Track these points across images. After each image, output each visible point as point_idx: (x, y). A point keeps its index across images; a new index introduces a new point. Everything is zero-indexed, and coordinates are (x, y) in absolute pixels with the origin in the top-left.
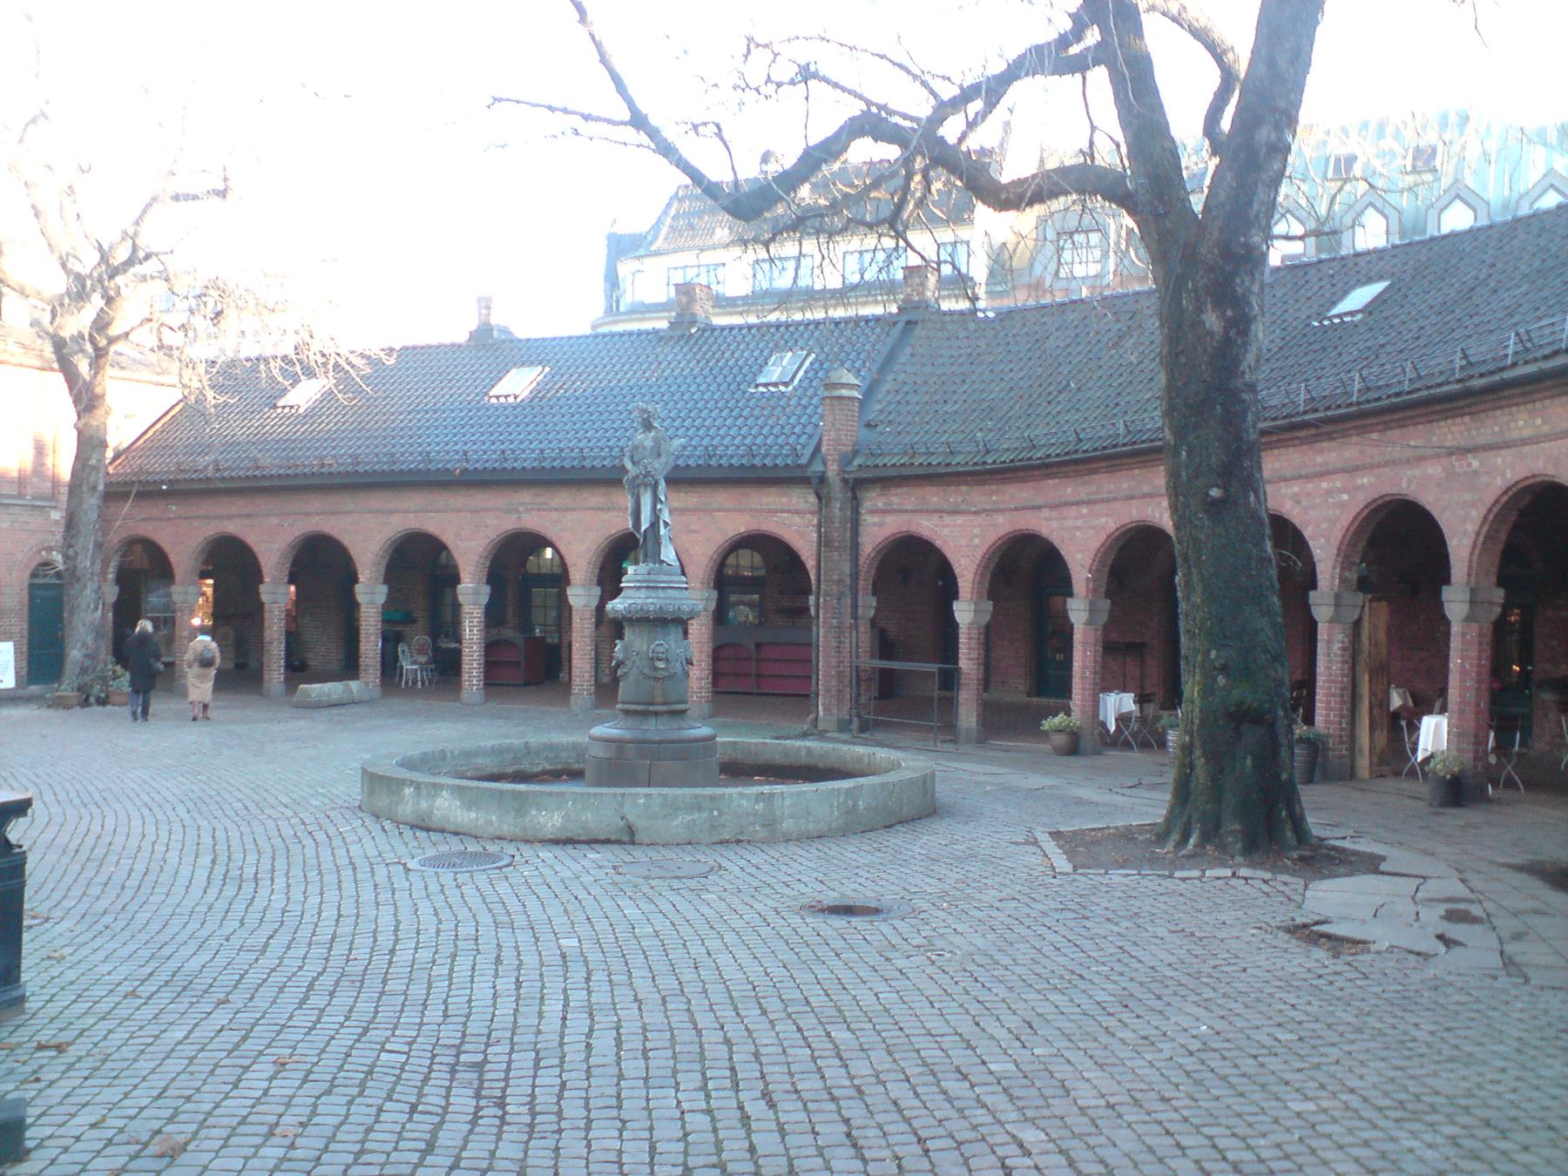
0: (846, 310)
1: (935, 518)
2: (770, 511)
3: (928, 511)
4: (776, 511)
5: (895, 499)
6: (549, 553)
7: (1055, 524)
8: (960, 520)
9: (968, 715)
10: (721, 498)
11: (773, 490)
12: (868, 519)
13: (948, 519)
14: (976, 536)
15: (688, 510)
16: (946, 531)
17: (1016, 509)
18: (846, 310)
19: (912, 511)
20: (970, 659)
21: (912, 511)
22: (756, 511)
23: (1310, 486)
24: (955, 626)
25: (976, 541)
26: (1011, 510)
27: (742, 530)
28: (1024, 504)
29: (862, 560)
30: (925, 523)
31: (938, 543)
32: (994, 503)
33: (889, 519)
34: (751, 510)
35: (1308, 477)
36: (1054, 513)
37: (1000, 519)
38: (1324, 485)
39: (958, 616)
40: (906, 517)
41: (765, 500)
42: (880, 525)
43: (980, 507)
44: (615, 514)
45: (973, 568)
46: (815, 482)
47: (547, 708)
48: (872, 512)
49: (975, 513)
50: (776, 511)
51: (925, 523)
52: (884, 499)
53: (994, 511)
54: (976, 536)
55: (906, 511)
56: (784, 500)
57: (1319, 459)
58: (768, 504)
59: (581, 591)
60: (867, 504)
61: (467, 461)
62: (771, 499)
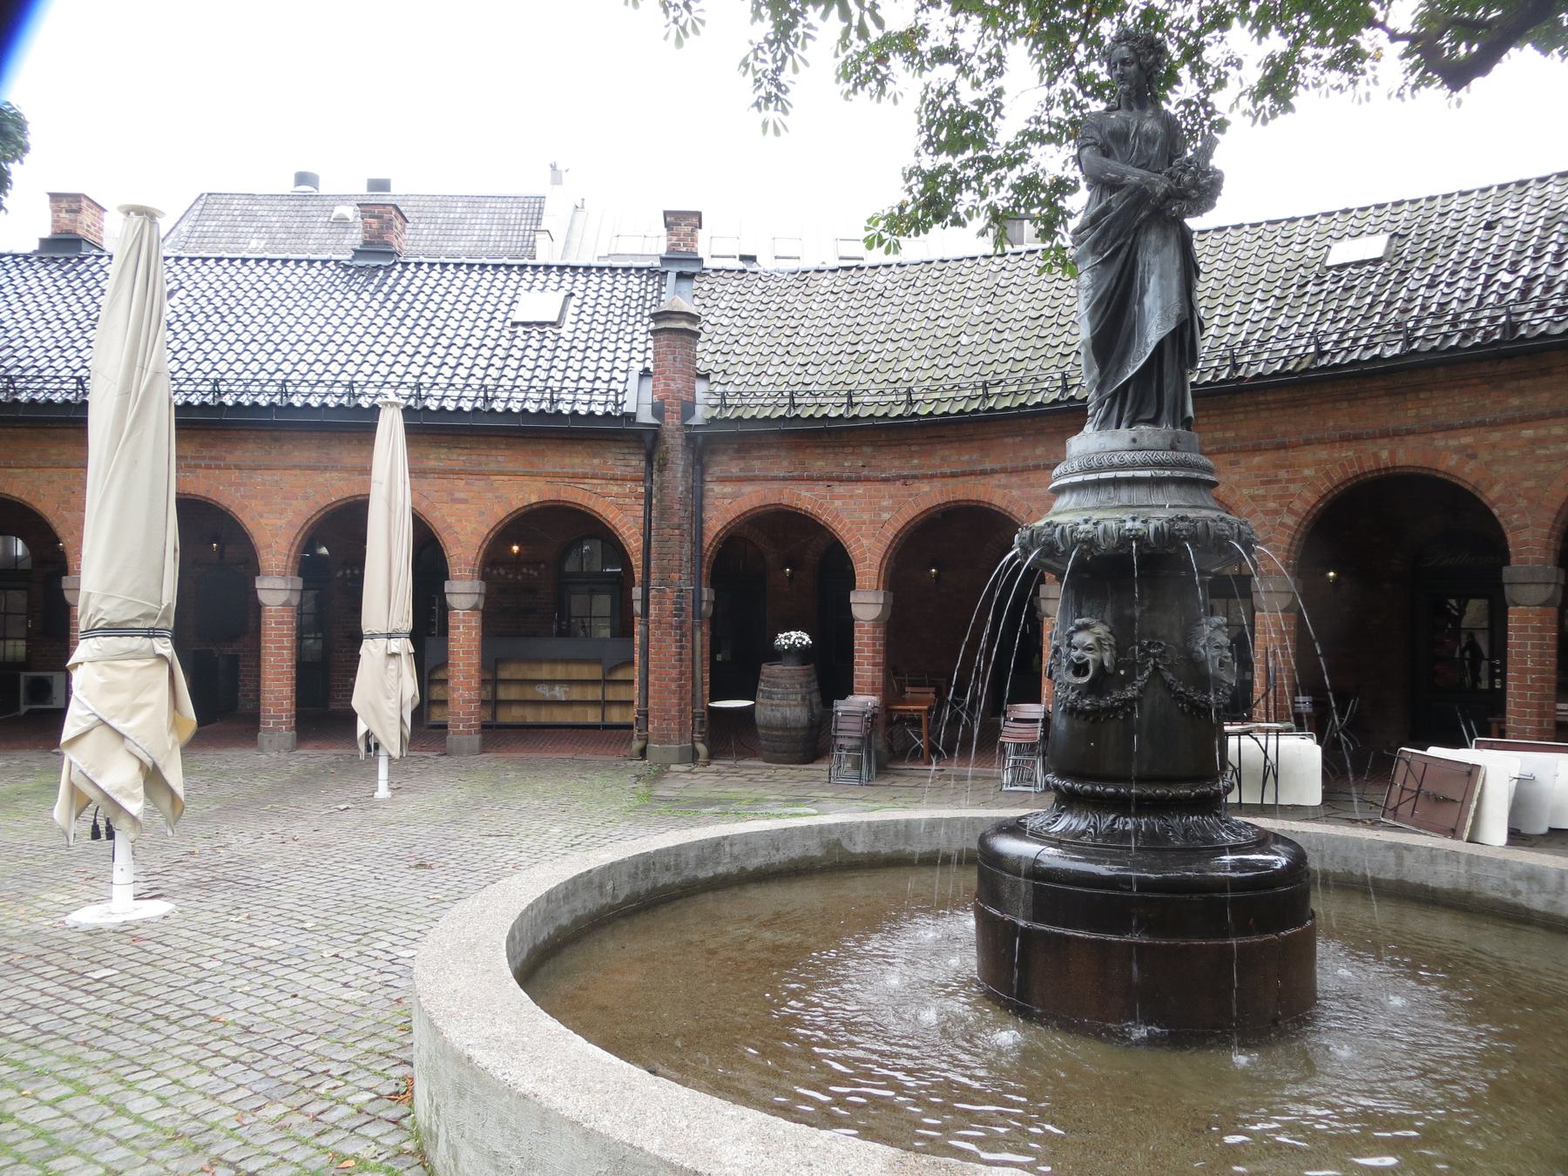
1: (820, 488)
2: (574, 476)
3: (810, 479)
4: (585, 476)
5: (757, 464)
6: (719, 657)
8: (859, 489)
9: (1133, 810)
10: (501, 458)
11: (23, 747)
12: (715, 489)
13: (839, 489)
15: (453, 472)
17: (954, 475)
19: (784, 479)
22: (556, 475)
23: (1496, 436)
25: (886, 516)
26: (943, 476)
27: (534, 499)
29: (707, 541)
31: (826, 518)
32: (915, 467)
33: (748, 489)
34: (547, 475)
36: (1014, 479)
37: (925, 487)
38: (1528, 433)
39: (857, 611)
40: (776, 485)
41: (567, 461)
42: (734, 496)
43: (894, 472)
44: (335, 474)
46: (648, 438)
48: (722, 480)
50: (585, 476)
51: (804, 493)
52: (742, 464)
53: (915, 477)
55: (774, 479)
56: (596, 461)
58: (573, 467)
59: (279, 583)
60: (715, 470)
62: (577, 461)
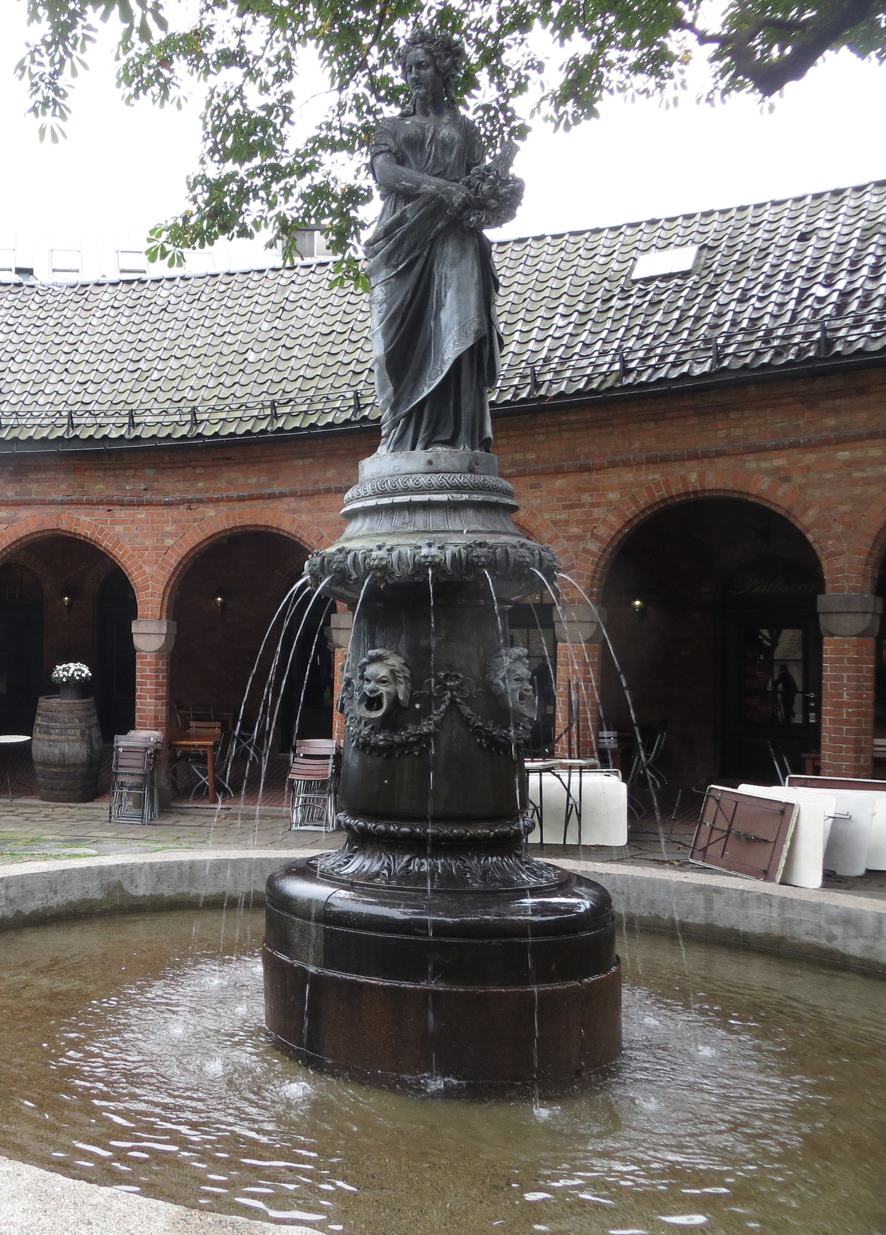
0: (292, 195)
1: (100, 513)
3: (90, 503)
5: (34, 487)
7: (305, 518)
8: (141, 514)
13: (121, 513)
14: (169, 535)
16: (119, 528)
18: (292, 195)
19: (63, 503)
20: (157, 698)
21: (63, 503)
23: (810, 458)
24: (129, 653)
25: (169, 542)
28: (255, 492)
30: (83, 518)
31: (106, 544)
32: (200, 491)
33: (24, 513)
35: (809, 446)
36: (304, 504)
37: (210, 512)
39: (139, 642)
40: (54, 510)
43: (178, 496)
45: (163, 577)
47: (37, 831)
49: (169, 504)
51: (83, 518)
53: (200, 501)
54: (169, 535)
57: (831, 422)
61: (275, 416)
